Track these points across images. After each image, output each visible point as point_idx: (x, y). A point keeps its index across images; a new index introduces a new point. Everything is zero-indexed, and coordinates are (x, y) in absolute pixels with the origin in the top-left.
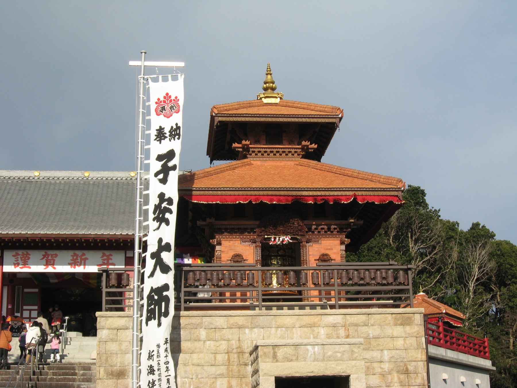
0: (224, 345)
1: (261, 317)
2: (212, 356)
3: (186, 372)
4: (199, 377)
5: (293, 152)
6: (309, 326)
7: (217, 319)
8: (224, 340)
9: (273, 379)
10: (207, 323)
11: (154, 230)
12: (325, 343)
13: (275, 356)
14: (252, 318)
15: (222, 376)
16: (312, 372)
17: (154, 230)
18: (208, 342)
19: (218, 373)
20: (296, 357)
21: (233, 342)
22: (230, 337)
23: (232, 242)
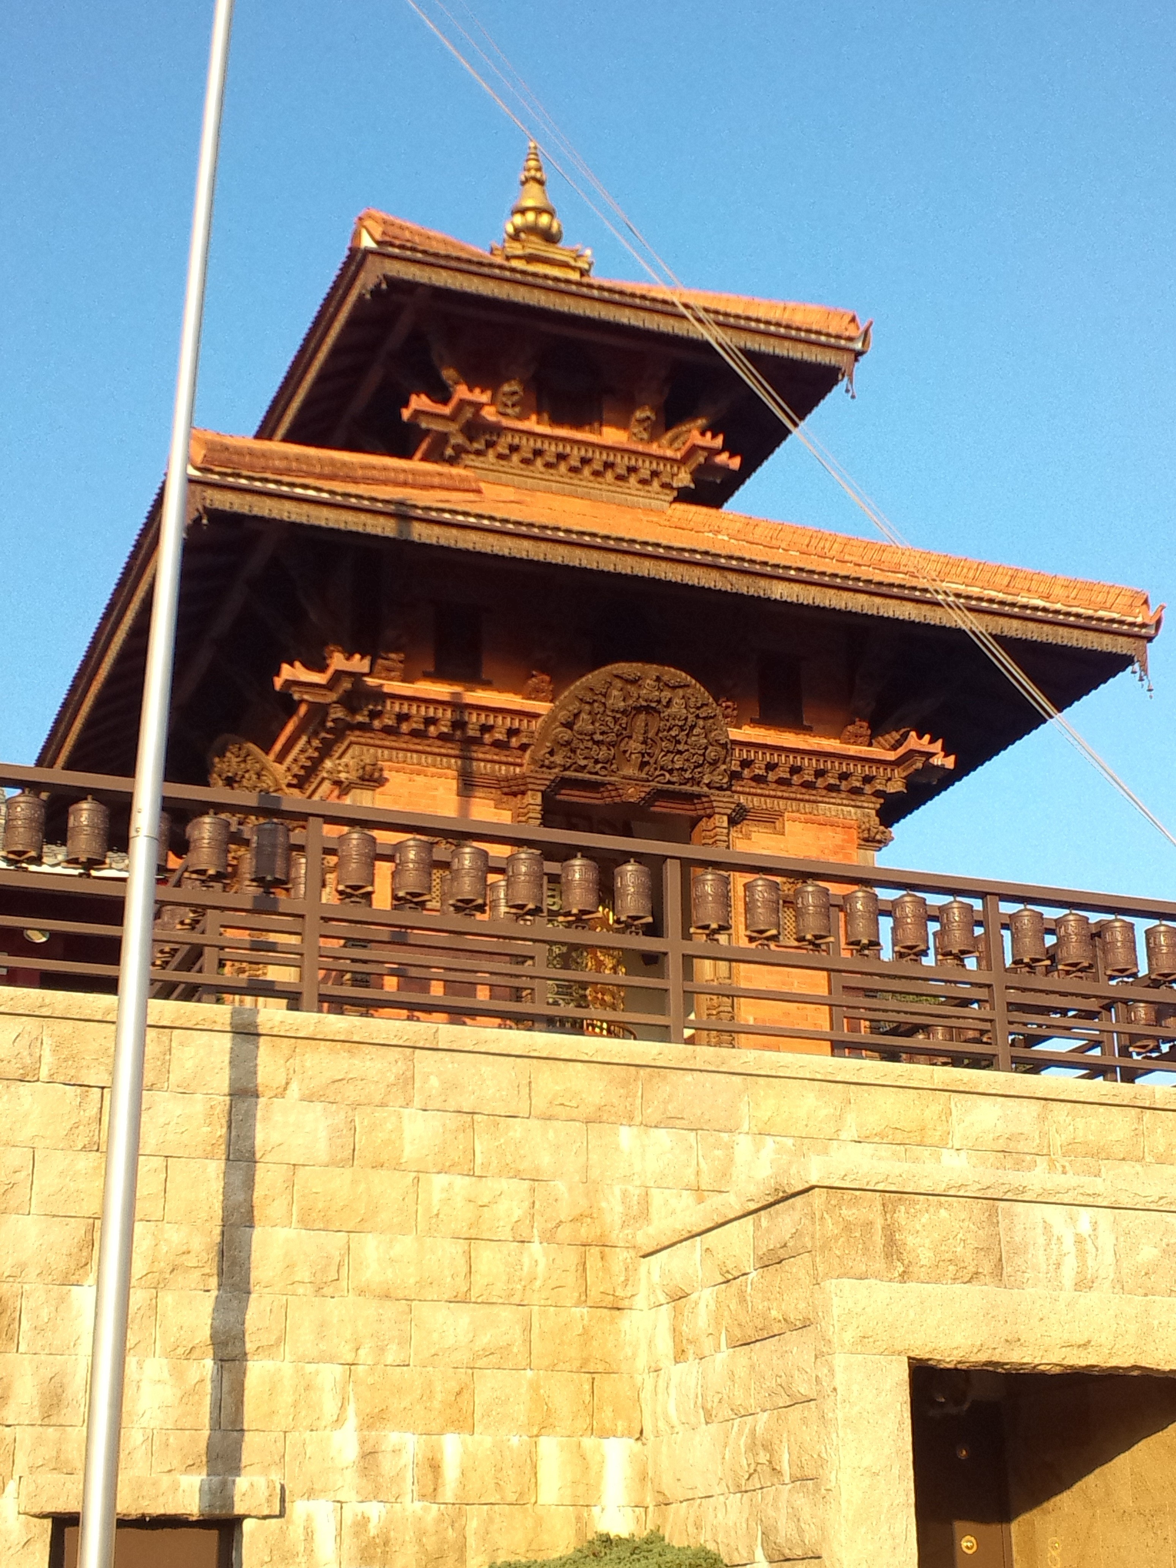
0: (510, 1203)
1: (689, 1077)
2: (456, 1249)
3: (322, 1328)
4: (390, 1359)
5: (645, 473)
6: (899, 1137)
7: (487, 1066)
8: (517, 1175)
9: (902, 1373)
10: (434, 1081)
11: (871, 324)
12: (1125, 1201)
13: (893, 1248)
14: (651, 1076)
15: (498, 1357)
16: (1086, 1345)
17: (871, 324)
18: (440, 1181)
19: (484, 1340)
20: (994, 1258)
21: (560, 1187)
22: (546, 1160)
23: (420, 779)
